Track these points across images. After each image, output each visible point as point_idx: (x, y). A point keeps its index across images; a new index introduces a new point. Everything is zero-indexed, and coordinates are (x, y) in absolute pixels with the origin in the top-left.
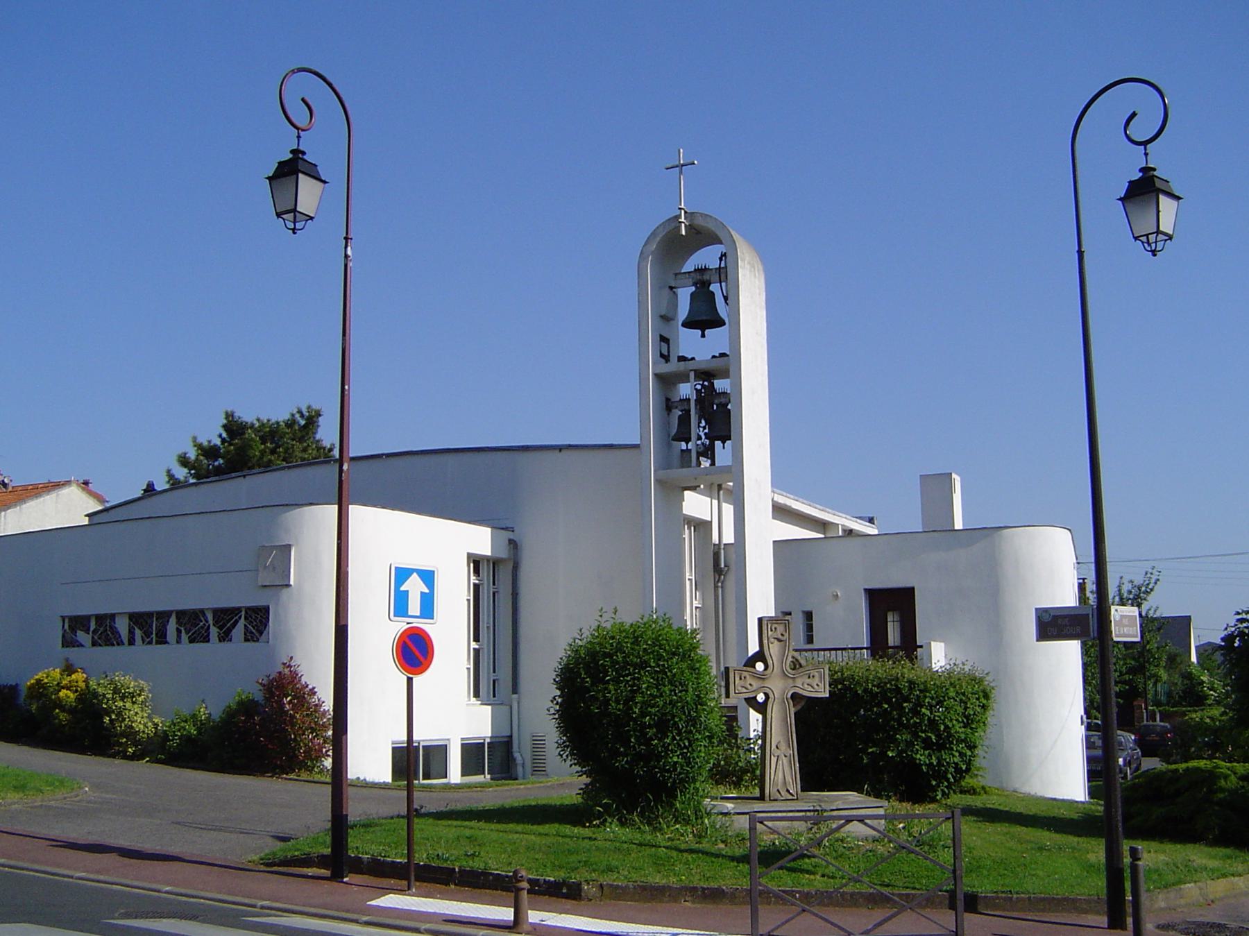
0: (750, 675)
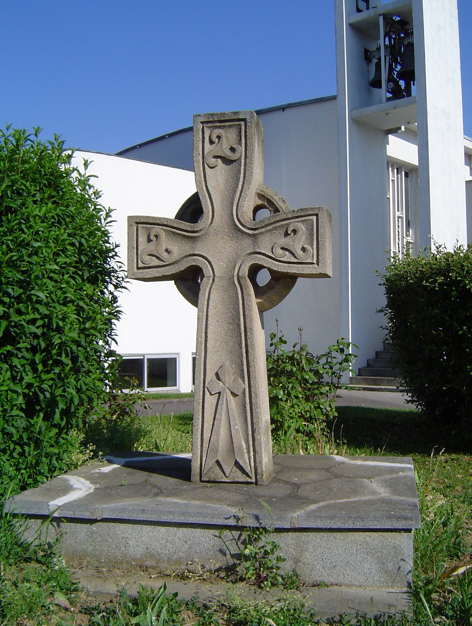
0: (164, 230)
